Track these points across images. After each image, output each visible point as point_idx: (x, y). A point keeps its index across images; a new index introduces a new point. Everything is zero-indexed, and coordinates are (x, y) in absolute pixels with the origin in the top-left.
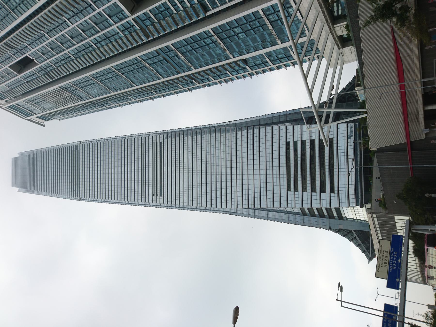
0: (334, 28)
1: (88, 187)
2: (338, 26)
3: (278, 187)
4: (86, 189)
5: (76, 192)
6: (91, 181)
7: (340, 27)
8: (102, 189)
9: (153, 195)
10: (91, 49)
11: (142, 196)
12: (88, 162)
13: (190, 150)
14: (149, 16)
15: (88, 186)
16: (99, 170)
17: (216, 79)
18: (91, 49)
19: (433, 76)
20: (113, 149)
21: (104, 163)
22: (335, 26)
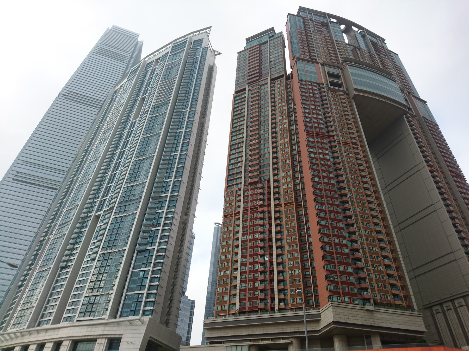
0: (106, 338)
1: (96, 64)
2: (105, 342)
3: (28, 211)
4: (96, 62)
5: (65, 95)
6: (101, 68)
7: (104, 343)
8: (86, 77)
9: (18, 172)
10: (184, 107)
11: (23, 161)
12: (109, 73)
13: (9, 230)
14: (169, 178)
15: (97, 64)
16: (74, 110)
17: (122, 198)
18: (184, 107)
19: (309, 347)
20: (72, 138)
21: (101, 89)
22: (107, 340)
